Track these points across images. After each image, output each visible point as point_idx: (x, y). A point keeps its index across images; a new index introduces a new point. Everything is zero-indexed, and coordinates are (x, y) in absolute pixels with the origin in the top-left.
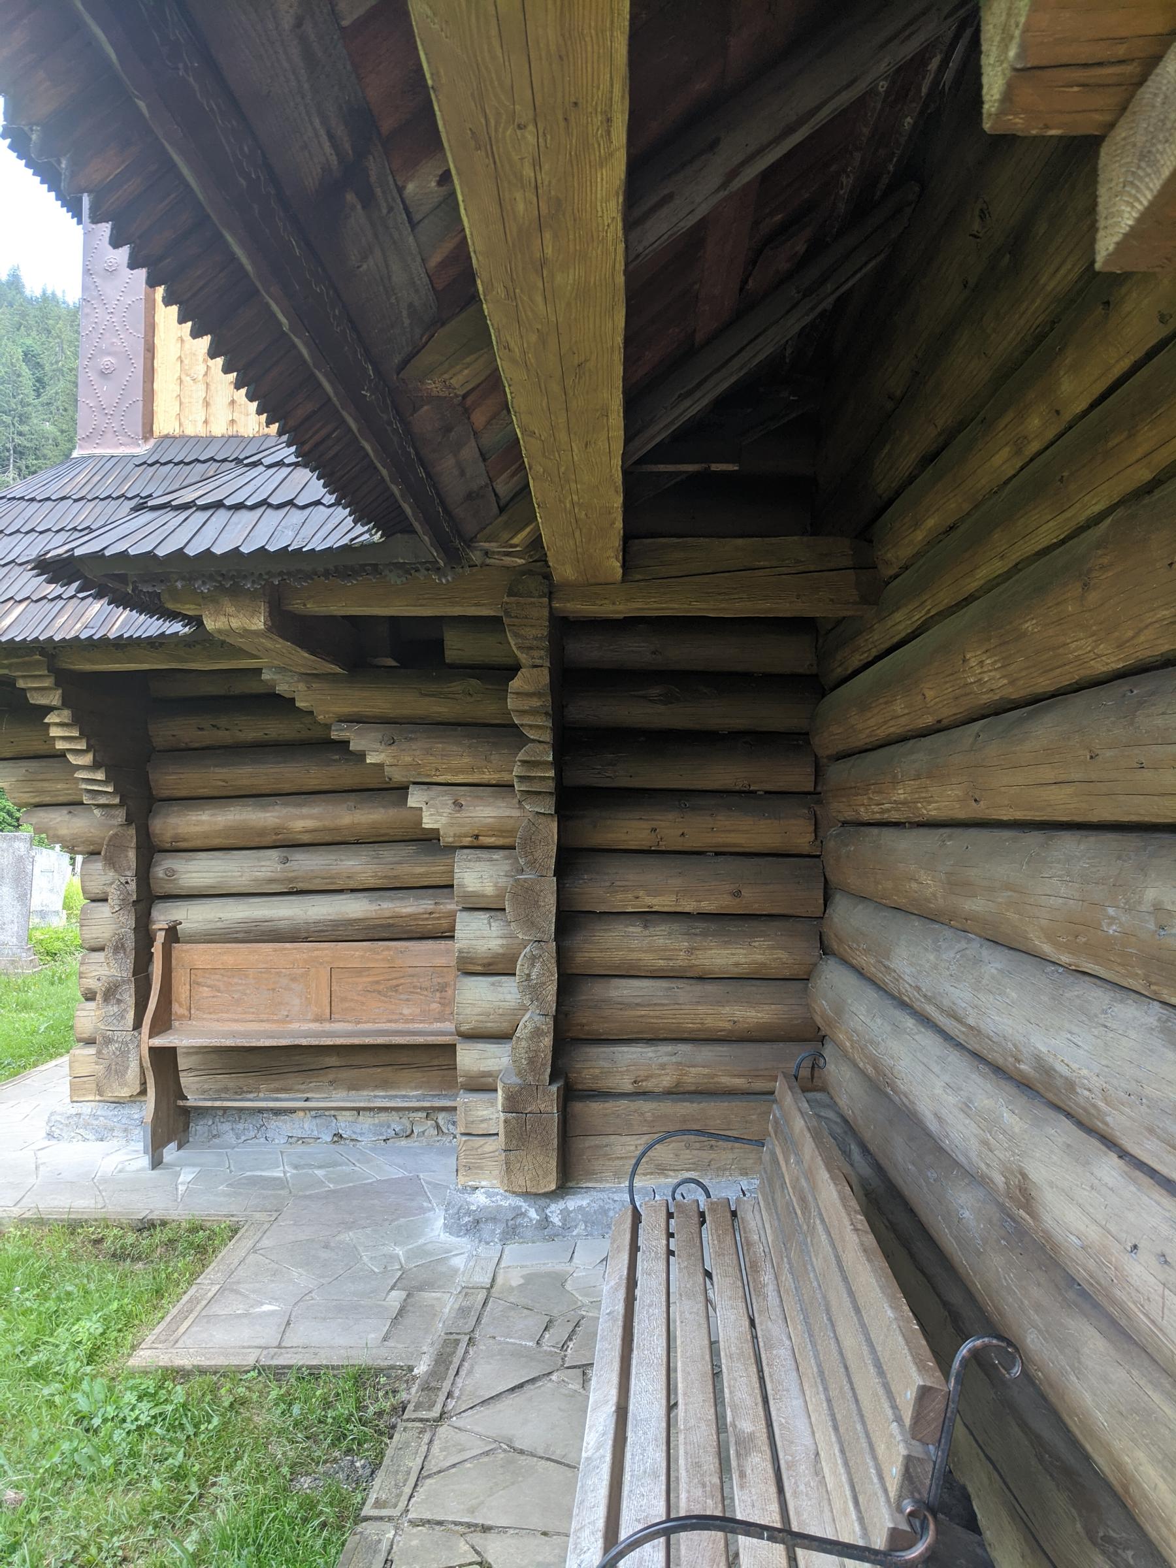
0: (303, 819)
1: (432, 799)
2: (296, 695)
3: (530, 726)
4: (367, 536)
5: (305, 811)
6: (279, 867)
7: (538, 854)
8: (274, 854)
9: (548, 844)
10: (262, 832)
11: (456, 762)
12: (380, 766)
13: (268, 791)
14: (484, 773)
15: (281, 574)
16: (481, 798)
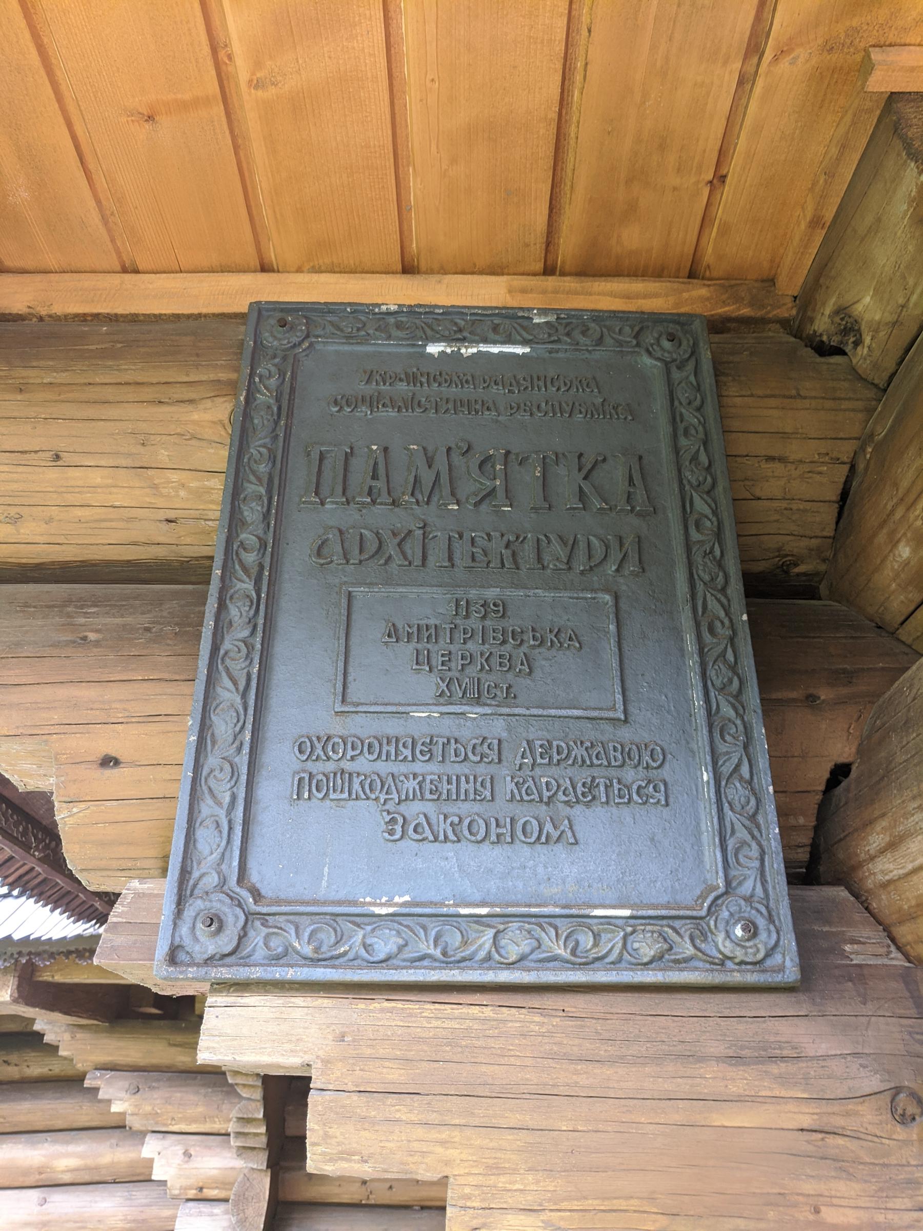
0: (65, 1156)
1: (165, 1148)
2: (60, 1044)
3: (244, 1085)
4: (91, 930)
5: (71, 1148)
6: (37, 1209)
7: (250, 1212)
8: (34, 1194)
9: (259, 1201)
10: (26, 1172)
11: (191, 1111)
12: (123, 1114)
13: (41, 1128)
14: (215, 1122)
15: (30, 953)
16: (209, 1148)
